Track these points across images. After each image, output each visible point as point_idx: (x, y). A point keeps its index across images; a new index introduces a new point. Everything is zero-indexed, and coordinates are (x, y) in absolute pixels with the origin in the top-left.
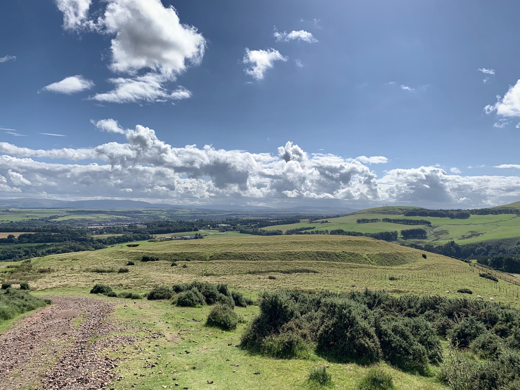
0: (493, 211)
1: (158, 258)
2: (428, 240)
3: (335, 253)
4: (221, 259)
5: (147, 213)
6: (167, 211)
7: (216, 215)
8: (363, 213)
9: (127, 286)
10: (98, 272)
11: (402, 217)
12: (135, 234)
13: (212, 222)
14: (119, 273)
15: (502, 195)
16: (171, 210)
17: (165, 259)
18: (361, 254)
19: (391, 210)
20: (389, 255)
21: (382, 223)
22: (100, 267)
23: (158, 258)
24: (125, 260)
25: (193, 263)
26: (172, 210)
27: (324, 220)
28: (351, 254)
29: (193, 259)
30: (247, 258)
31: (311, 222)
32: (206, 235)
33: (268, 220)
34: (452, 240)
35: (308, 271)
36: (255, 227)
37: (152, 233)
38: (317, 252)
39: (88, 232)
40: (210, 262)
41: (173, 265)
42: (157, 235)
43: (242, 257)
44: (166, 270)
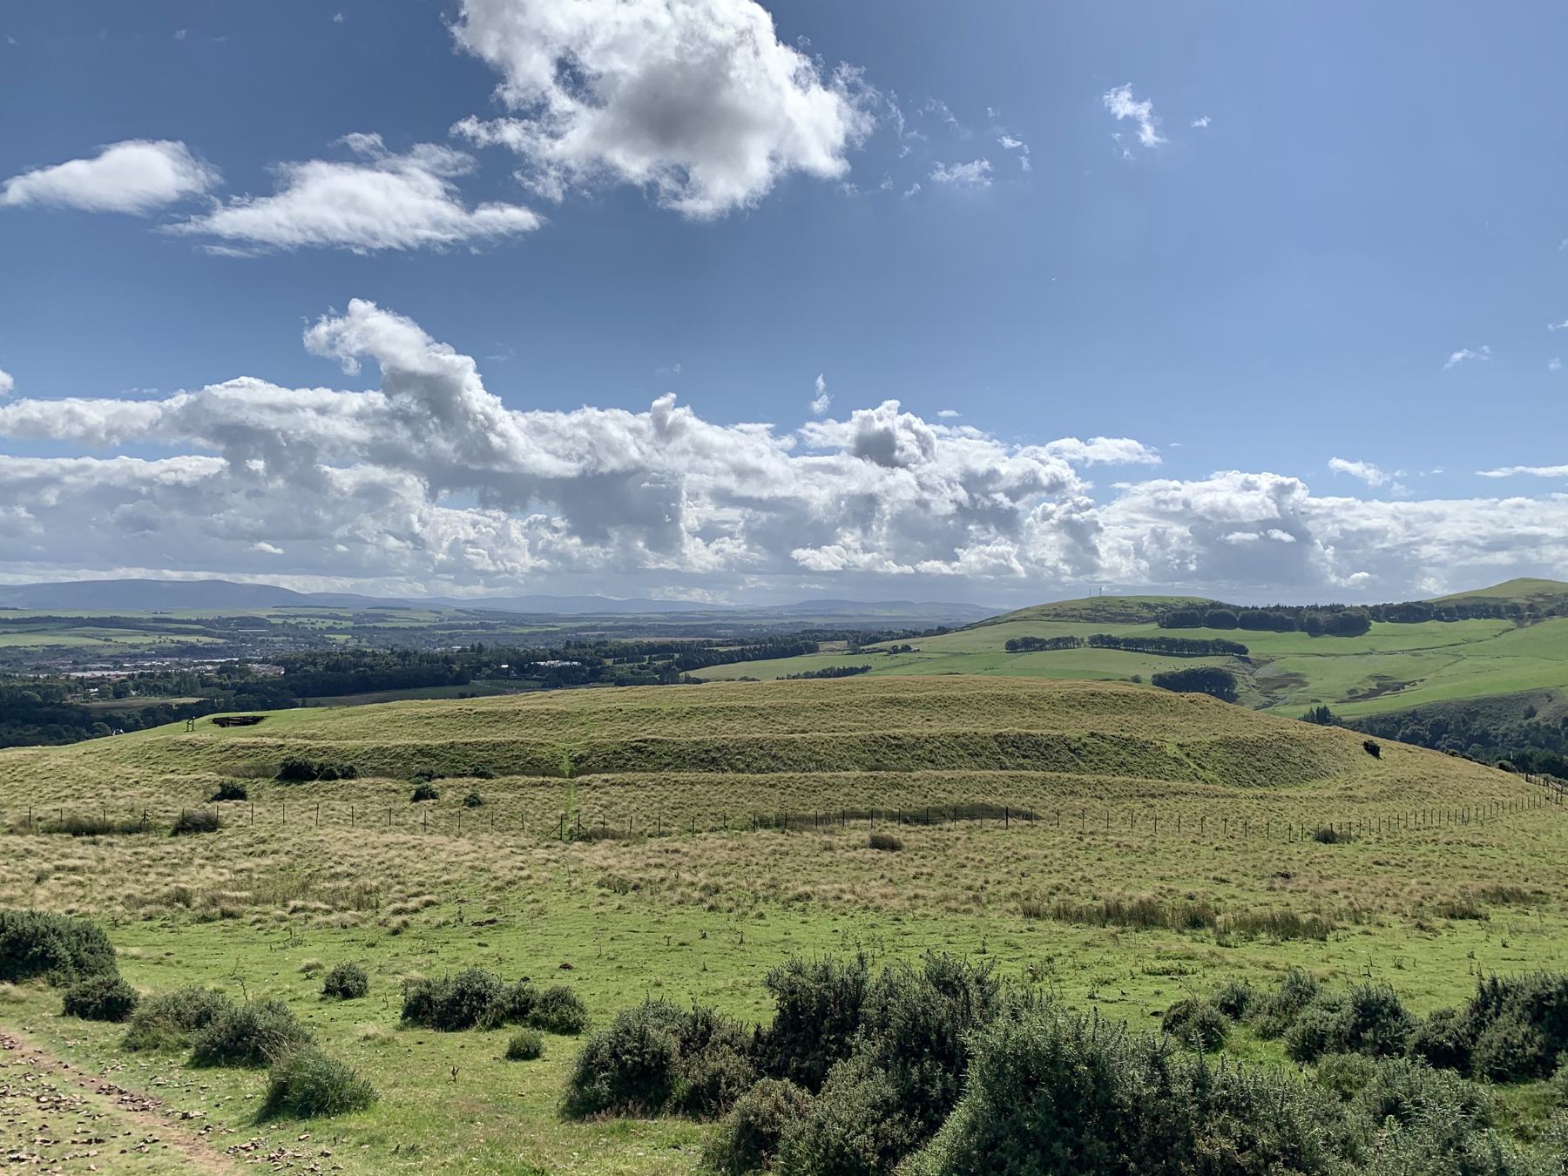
0: (1440, 612)
3: (1064, 741)
4: (622, 768)
7: (526, 631)
9: (214, 902)
10: (76, 834)
11: (1150, 630)
13: (515, 652)
14: (175, 834)
15: (1476, 561)
16: (367, 615)
17: (378, 772)
18: (1158, 743)
19: (1114, 610)
21: (1089, 650)
22: (86, 809)
23: (351, 769)
24: (206, 776)
25: (507, 788)
27: (900, 643)
28: (1125, 743)
29: (506, 771)
30: (730, 765)
31: (855, 652)
33: (709, 644)
34: (1321, 706)
35: (1006, 813)
38: (996, 737)
39: (70, 690)
40: (579, 779)
41: (419, 796)
43: (709, 759)
44: (394, 819)
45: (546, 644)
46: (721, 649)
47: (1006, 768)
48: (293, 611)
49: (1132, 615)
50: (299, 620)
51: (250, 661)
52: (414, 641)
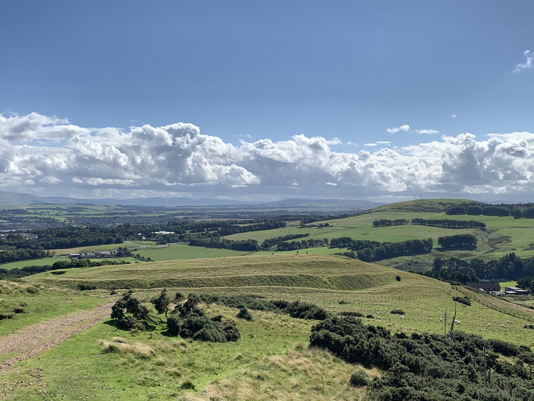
1: (95, 287)
2: (479, 251)
5: (34, 213)
6: (70, 210)
7: (150, 215)
8: (384, 210)
11: (441, 216)
12: (21, 250)
13: (144, 227)
16: (74, 208)
17: (101, 288)
19: (427, 206)
20: (353, 278)
26: (78, 208)
27: (324, 222)
28: (309, 278)
30: (192, 285)
31: (302, 226)
32: (136, 250)
36: (215, 235)
37: (48, 248)
38: (270, 277)
40: (151, 289)
41: (112, 294)
42: (56, 250)
45: (160, 222)
46: (241, 226)
47: (271, 285)
48: (39, 206)
49: (434, 208)
50: (42, 210)
51: (20, 232)
52: (97, 221)
